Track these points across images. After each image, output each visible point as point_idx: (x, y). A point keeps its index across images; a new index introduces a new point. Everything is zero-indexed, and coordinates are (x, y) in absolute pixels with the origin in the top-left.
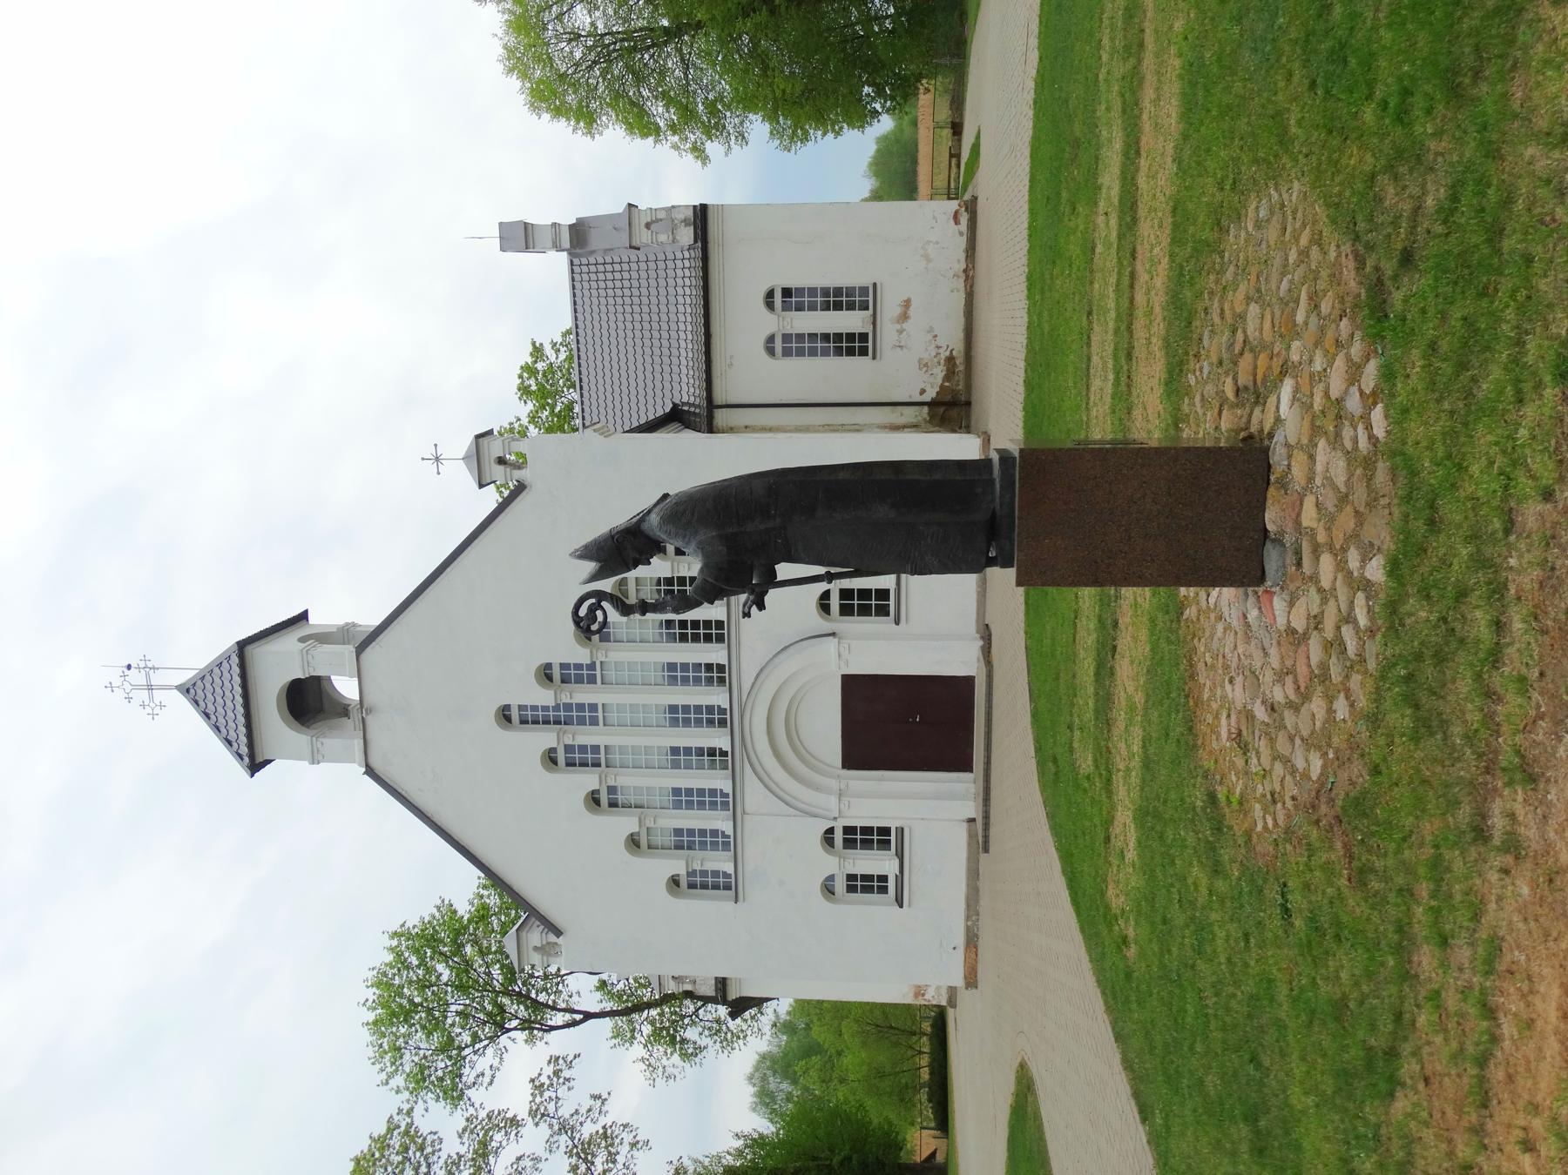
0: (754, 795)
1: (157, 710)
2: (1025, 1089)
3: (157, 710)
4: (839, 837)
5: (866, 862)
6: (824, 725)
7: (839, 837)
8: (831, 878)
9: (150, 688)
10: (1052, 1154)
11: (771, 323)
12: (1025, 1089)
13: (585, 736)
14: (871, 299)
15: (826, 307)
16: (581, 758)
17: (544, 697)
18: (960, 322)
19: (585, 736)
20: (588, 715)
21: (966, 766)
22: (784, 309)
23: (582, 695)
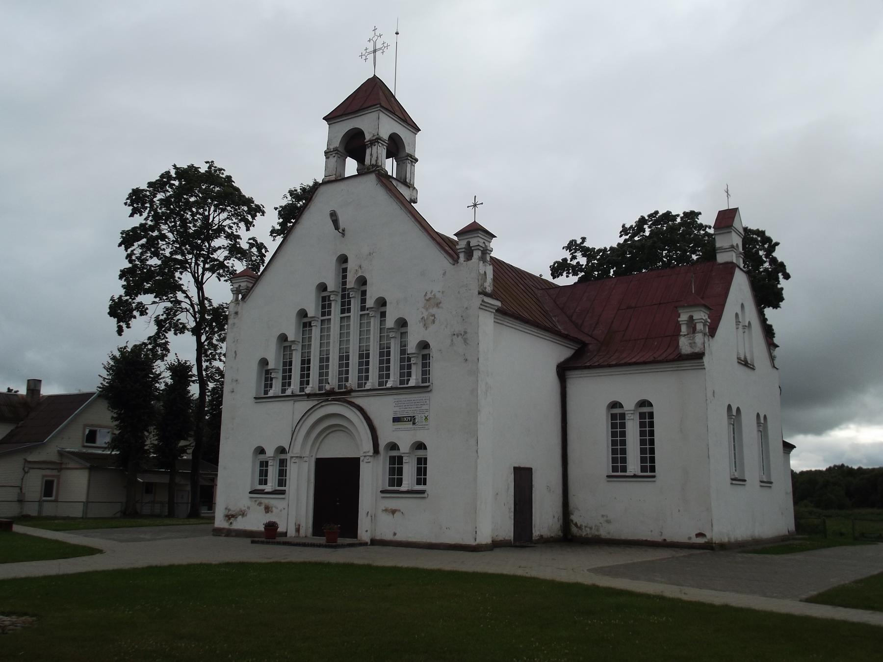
0: (304, 406)
1: (364, 57)
2: (100, 551)
3: (364, 57)
4: (646, 410)
5: (270, 467)
6: (336, 448)
7: (646, 410)
8: (621, 406)
9: (375, 51)
10: (116, 567)
11: (629, 405)
12: (100, 551)
13: (336, 308)
14: (619, 474)
15: (266, 475)
16: (325, 304)
17: (351, 282)
18: (626, 533)
19: (336, 308)
20: (345, 308)
21: (318, 527)
22: (641, 414)
23: (355, 305)
